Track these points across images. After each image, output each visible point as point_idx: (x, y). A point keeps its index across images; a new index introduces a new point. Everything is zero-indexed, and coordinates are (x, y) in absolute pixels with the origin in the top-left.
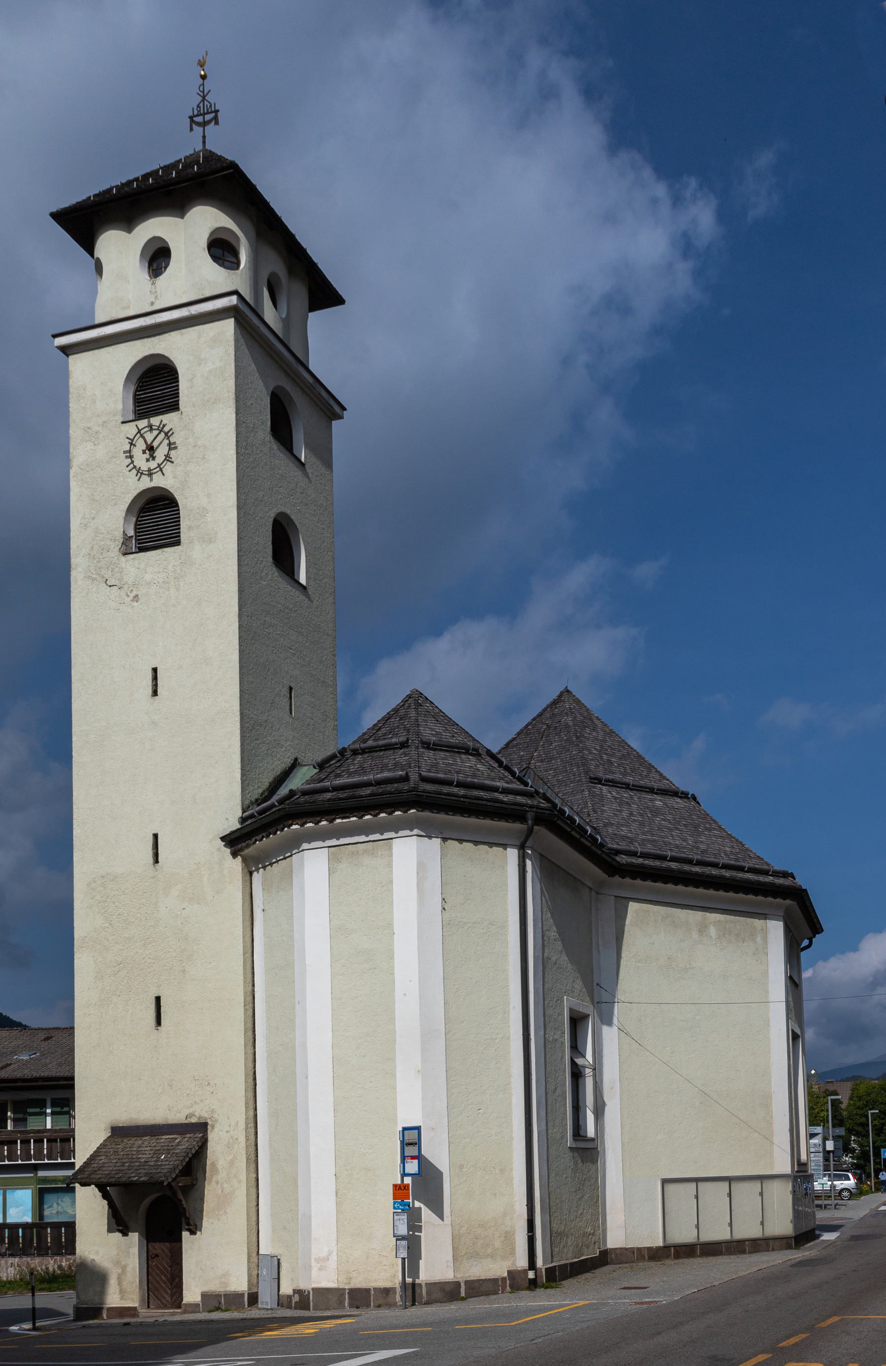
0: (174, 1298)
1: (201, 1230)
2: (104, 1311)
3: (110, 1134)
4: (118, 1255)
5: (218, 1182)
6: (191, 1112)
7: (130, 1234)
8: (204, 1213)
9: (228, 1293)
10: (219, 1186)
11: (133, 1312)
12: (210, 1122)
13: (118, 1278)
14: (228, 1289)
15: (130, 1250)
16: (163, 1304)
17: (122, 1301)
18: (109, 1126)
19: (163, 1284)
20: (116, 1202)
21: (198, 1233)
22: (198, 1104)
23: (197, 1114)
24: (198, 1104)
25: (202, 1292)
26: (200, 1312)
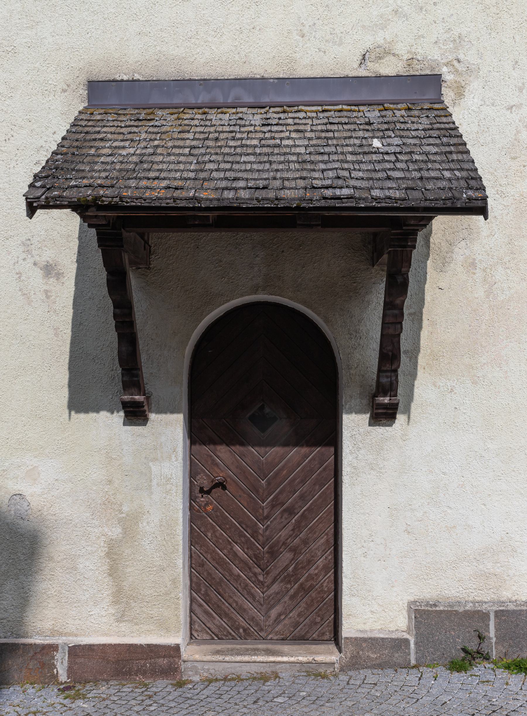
0: (274, 613)
1: (407, 411)
2: (58, 656)
3: (86, 105)
4: (110, 482)
5: (473, 264)
6: (381, 41)
7: (152, 416)
8: (422, 360)
9: (511, 607)
10: (479, 274)
11: (163, 662)
12: (448, 77)
13: (108, 554)
14: (506, 594)
15: (155, 468)
16: (236, 628)
17: (124, 627)
18: (83, 78)
19: (237, 571)
20: (397, 98)
21: (401, 418)
22: (406, 17)
23: (401, 49)
24: (406, 17)
25: (410, 604)
26: (407, 666)
